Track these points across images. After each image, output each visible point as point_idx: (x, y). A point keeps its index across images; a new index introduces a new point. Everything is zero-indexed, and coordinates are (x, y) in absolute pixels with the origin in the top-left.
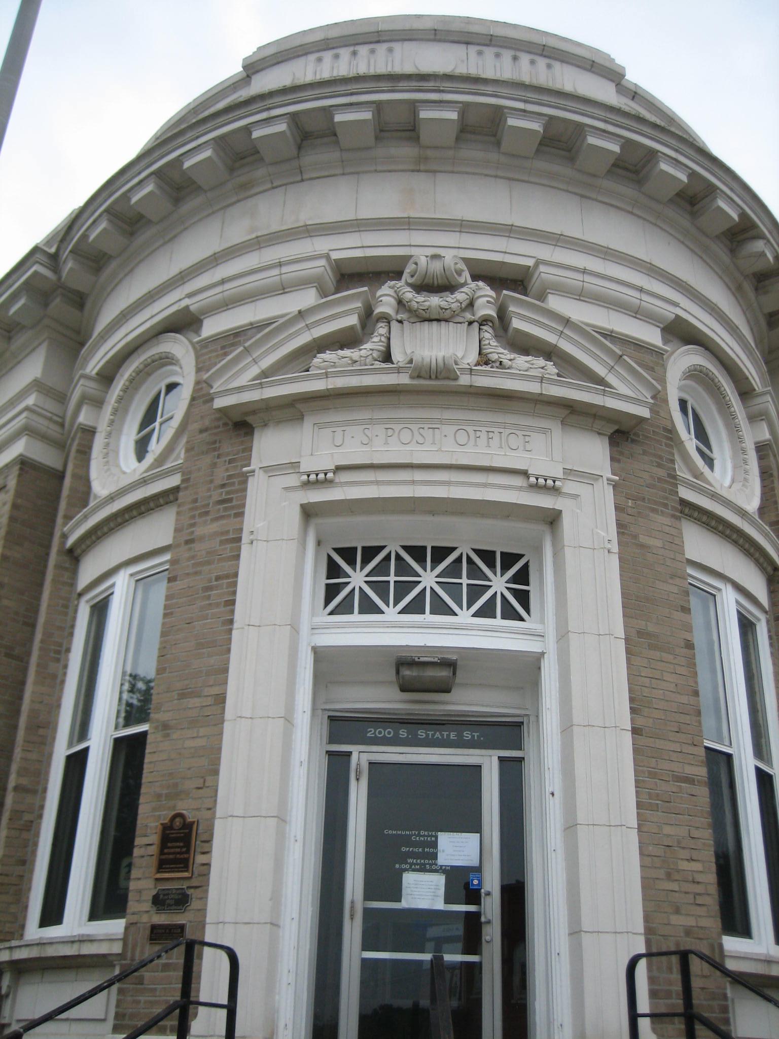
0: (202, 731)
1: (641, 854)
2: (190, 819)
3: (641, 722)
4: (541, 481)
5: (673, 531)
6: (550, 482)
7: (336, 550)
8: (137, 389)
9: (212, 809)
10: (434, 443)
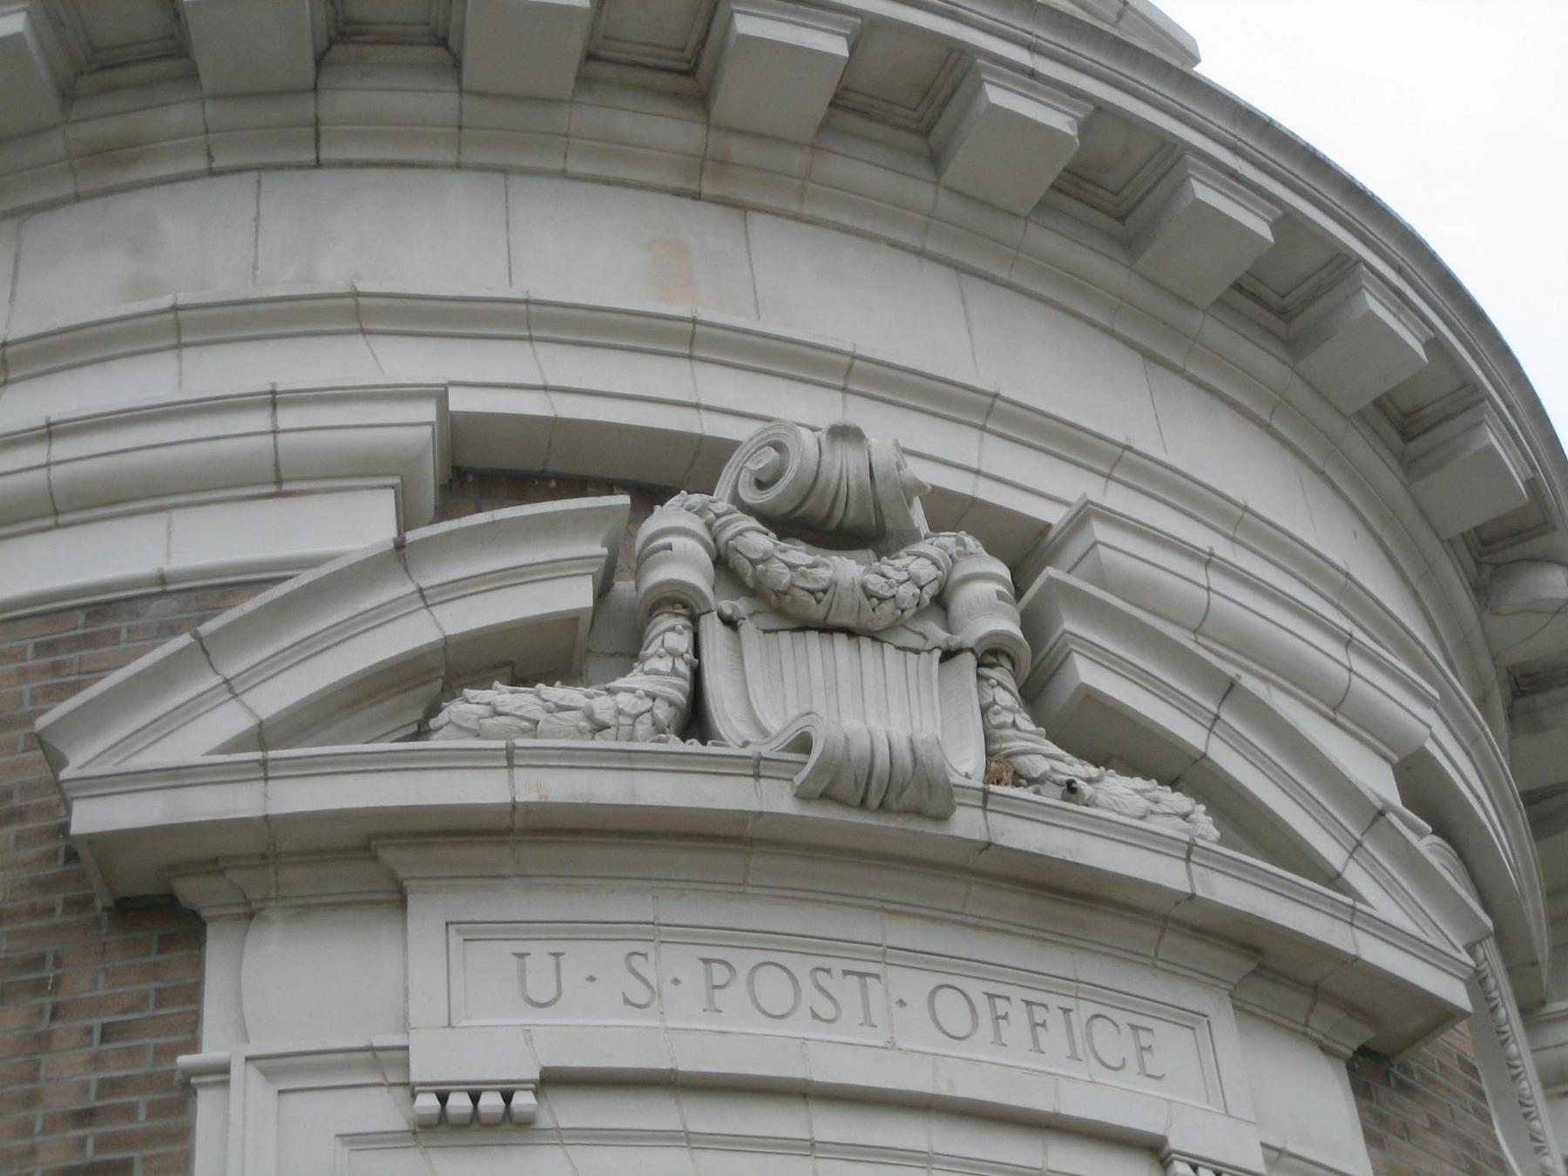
10: (868, 1022)
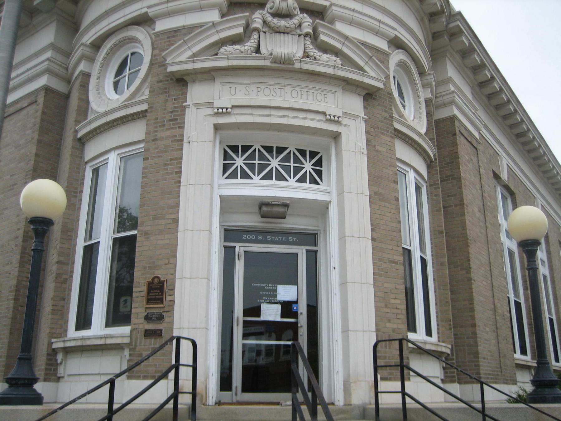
0: (166, 236)
1: (375, 296)
2: (162, 279)
3: (375, 235)
4: (332, 118)
5: (391, 144)
6: (336, 118)
7: (228, 146)
8: (114, 54)
9: (174, 274)
10: (281, 96)
